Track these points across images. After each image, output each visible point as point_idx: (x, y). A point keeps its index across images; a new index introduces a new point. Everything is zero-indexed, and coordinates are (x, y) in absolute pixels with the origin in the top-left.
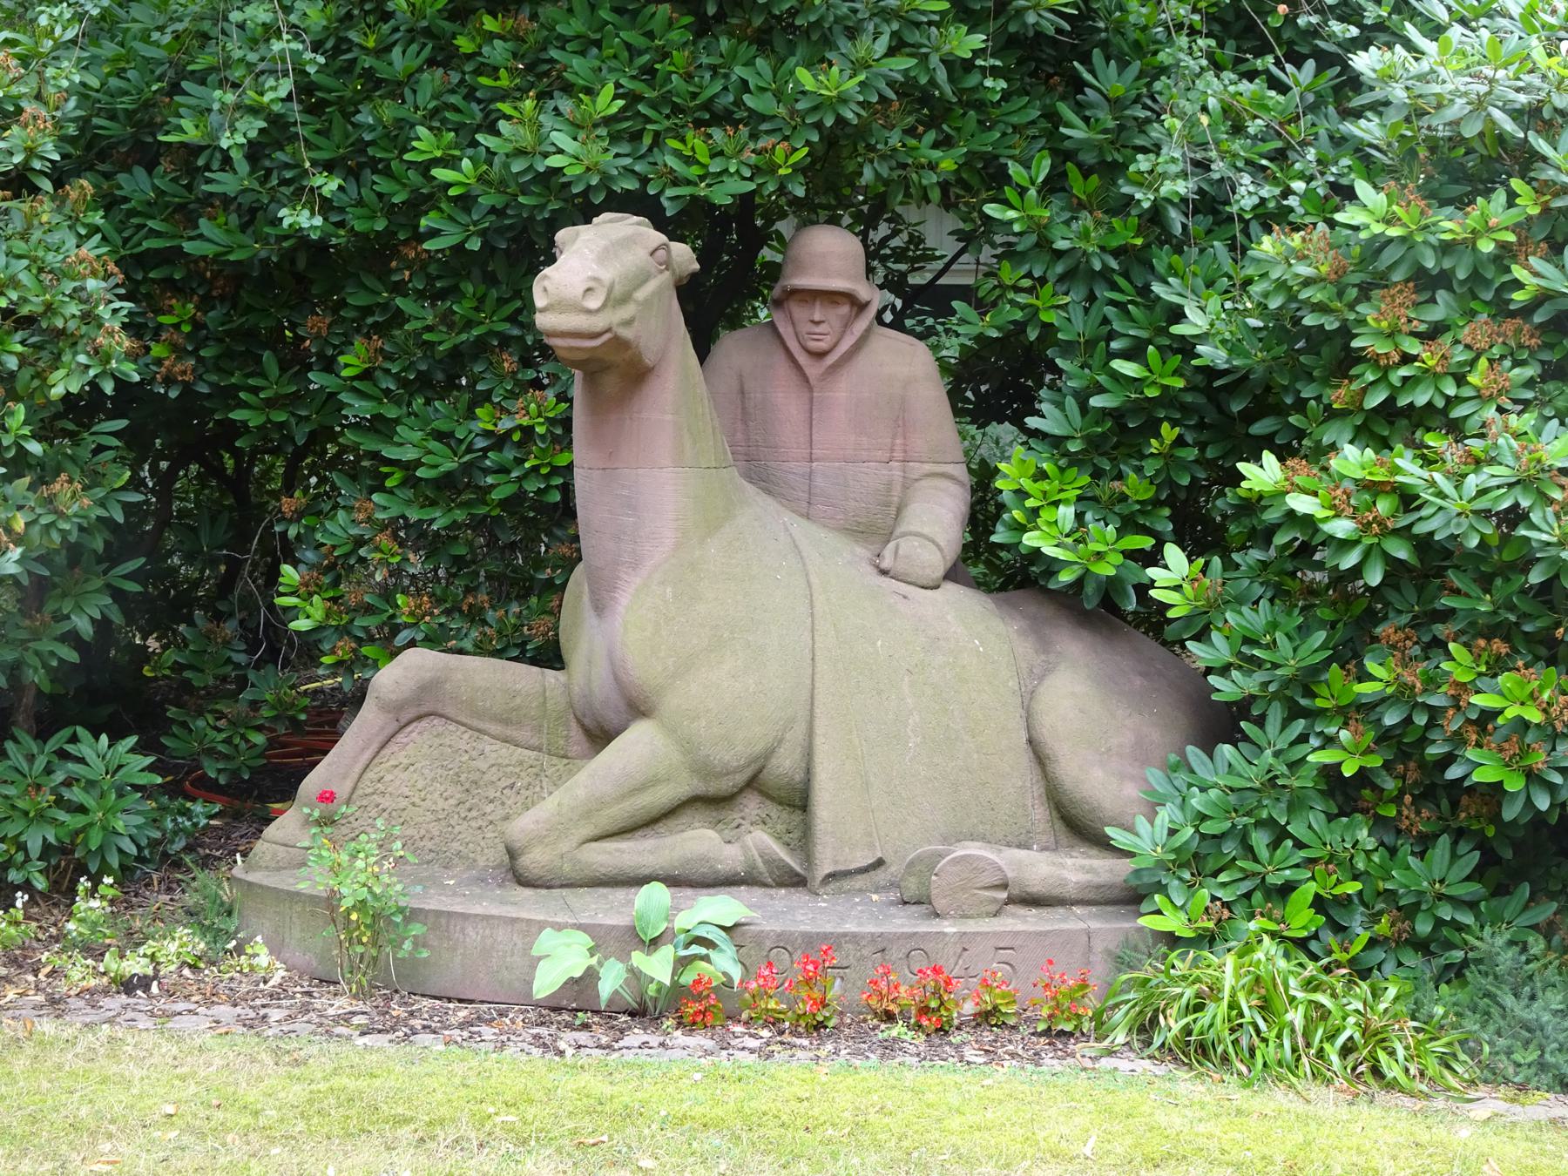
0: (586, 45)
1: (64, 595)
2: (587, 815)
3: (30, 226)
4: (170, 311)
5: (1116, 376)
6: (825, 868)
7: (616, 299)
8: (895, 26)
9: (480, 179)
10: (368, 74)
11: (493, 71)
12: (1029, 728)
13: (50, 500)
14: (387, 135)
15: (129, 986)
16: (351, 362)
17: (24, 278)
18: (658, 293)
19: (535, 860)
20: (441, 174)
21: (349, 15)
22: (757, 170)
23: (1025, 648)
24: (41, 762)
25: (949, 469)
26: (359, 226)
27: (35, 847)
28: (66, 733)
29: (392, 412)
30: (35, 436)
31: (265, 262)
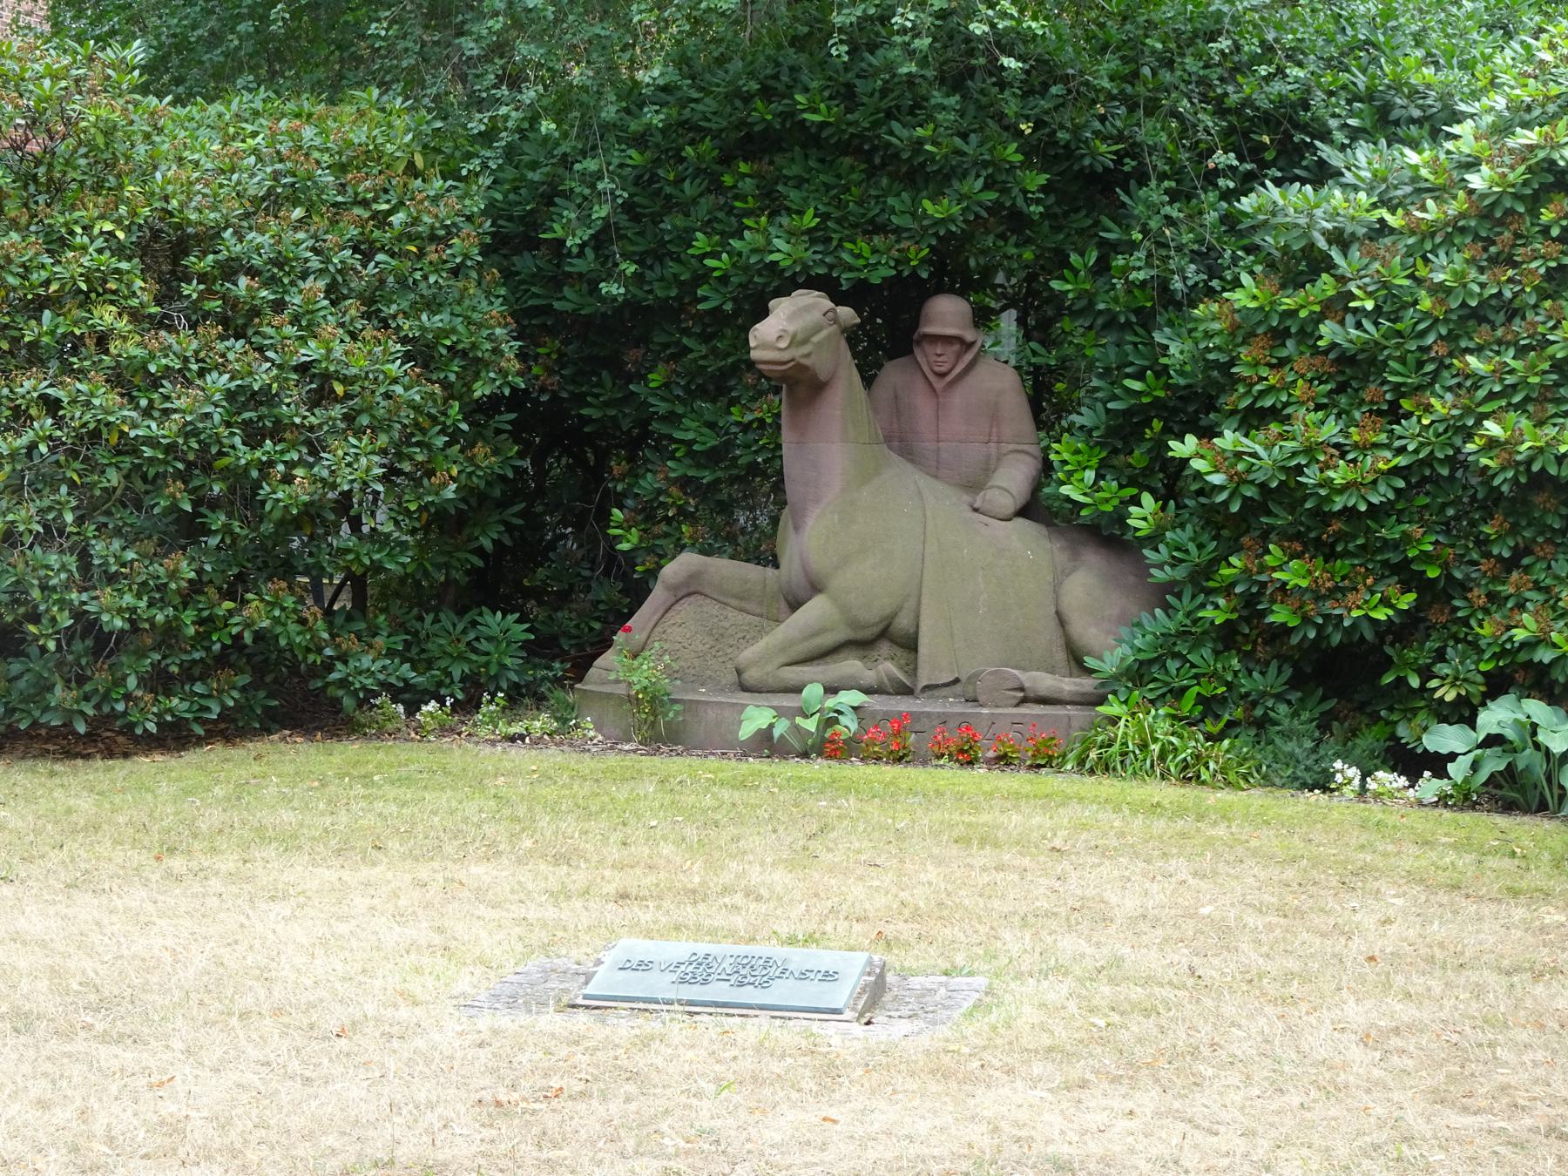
0: (800, 183)
1: (475, 525)
2: (783, 649)
3: (462, 297)
4: (544, 345)
5: (1128, 390)
6: (923, 682)
7: (795, 342)
8: (990, 171)
9: (734, 265)
10: (669, 197)
11: (744, 199)
12: (1057, 605)
13: (471, 460)
14: (679, 237)
15: (512, 739)
16: (655, 379)
17: (460, 328)
18: (829, 337)
19: (752, 675)
20: (710, 262)
21: (658, 159)
22: (898, 262)
23: (1062, 558)
24: (460, 627)
25: (1026, 447)
26: (659, 293)
27: (457, 674)
28: (475, 611)
29: (680, 410)
30: (465, 419)
31: (604, 315)
